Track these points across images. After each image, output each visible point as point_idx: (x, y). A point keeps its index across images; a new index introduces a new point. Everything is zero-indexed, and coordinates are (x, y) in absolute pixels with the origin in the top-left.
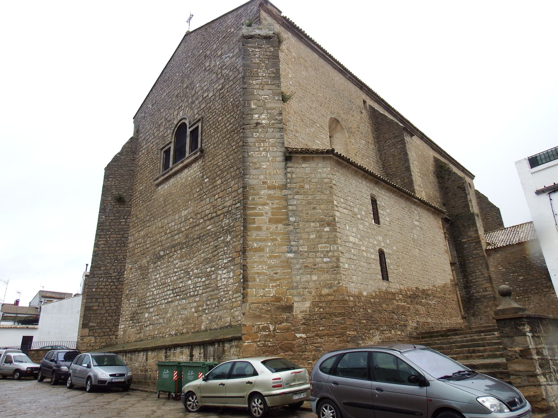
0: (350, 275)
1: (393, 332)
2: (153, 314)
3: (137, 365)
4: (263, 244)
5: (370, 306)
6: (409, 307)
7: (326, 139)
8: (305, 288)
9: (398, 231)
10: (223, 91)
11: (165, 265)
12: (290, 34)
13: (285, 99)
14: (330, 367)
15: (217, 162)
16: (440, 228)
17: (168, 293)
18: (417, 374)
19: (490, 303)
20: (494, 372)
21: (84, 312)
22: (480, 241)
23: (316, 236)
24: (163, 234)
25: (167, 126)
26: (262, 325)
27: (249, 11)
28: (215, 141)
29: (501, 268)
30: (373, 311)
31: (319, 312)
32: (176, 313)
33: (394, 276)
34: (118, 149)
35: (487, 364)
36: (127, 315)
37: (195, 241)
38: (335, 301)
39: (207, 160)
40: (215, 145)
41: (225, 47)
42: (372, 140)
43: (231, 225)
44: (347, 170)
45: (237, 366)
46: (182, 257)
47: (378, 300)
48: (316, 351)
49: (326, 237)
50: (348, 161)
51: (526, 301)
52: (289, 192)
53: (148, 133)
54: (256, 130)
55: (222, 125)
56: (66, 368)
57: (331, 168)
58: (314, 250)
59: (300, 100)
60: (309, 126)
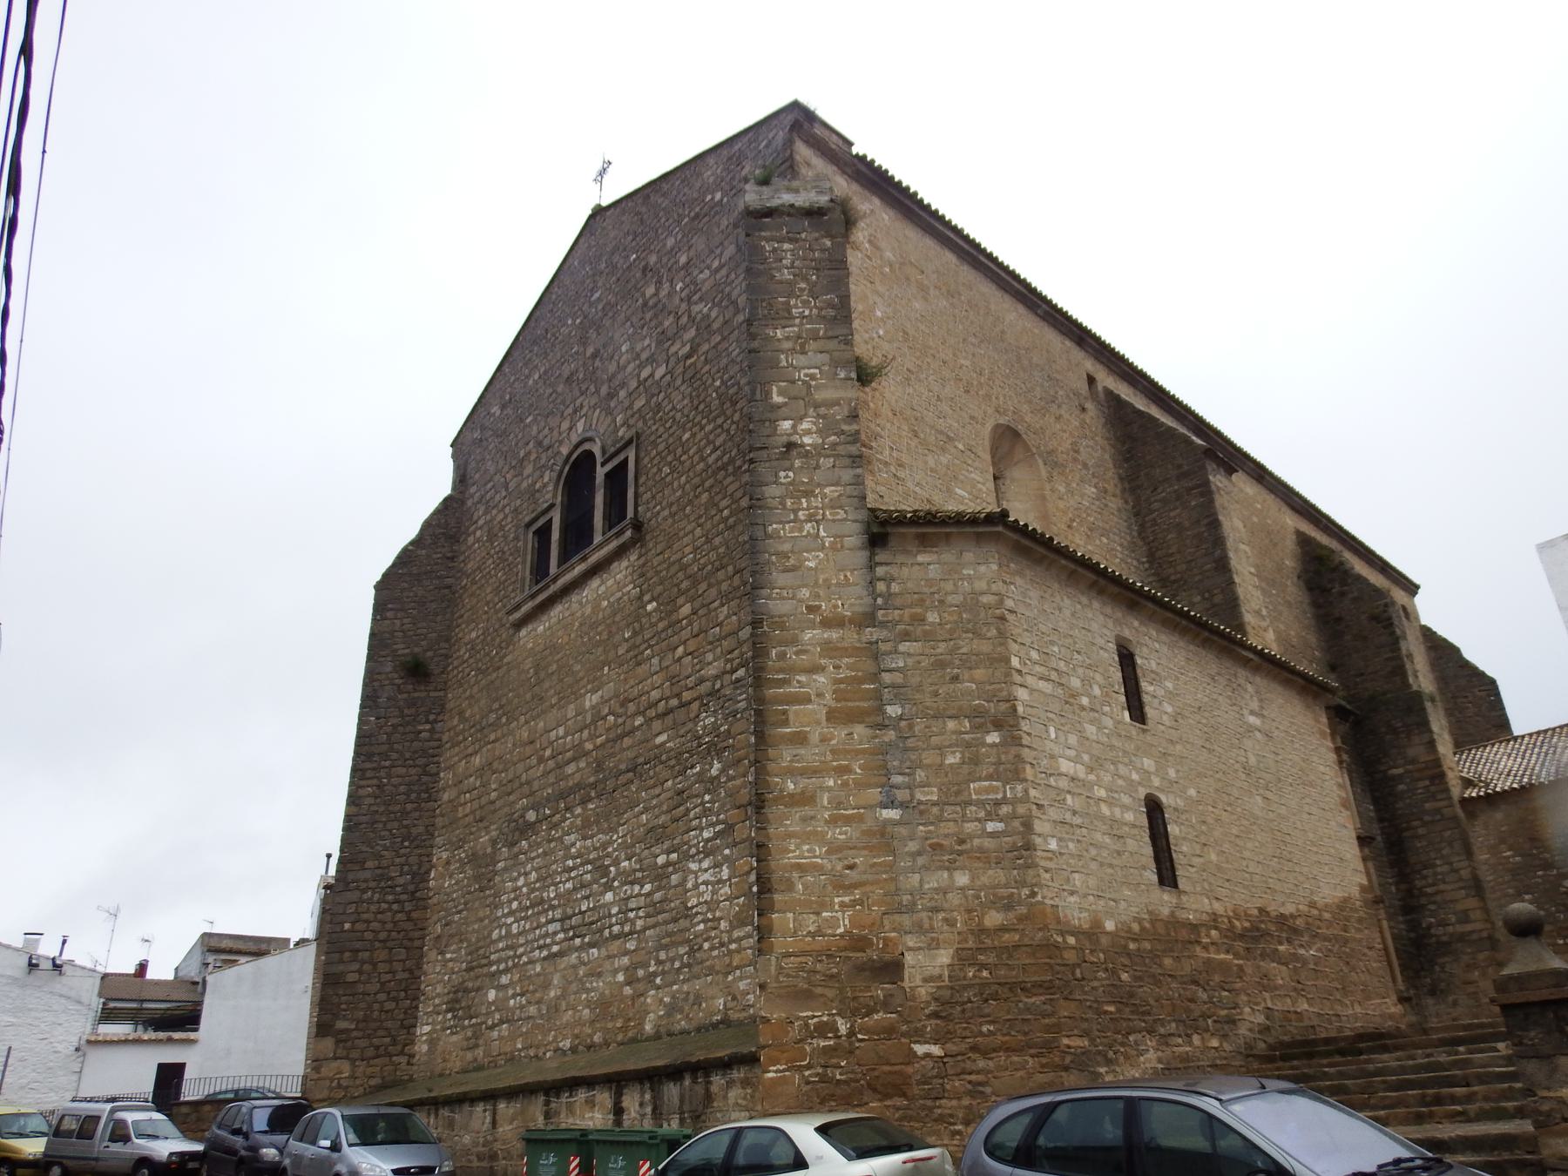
0: (1063, 872)
1: (1196, 1039)
2: (510, 992)
3: (467, 1139)
4: (813, 784)
5: (1127, 962)
6: (1240, 967)
7: (984, 484)
8: (936, 910)
9: (1201, 743)
10: (692, 360)
11: (540, 851)
12: (877, 201)
13: (865, 376)
14: (1014, 1144)
15: (679, 555)
16: (1322, 733)
17: (551, 928)
18: (1272, 1168)
19: (1481, 956)
20: (1498, 1162)
21: (323, 989)
22: (1442, 775)
23: (963, 757)
24: (534, 761)
25: (543, 462)
26: (816, 1020)
27: (764, 143)
28: (672, 499)
29: (1508, 853)
30: (1136, 978)
31: (977, 981)
32: (574, 987)
33: (1194, 875)
34: (411, 531)
35: (1476, 1136)
36: (438, 995)
37: (623, 779)
38: (1024, 949)
39: (653, 552)
40: (674, 508)
41: (699, 243)
42: (1116, 486)
43: (722, 729)
44: (1047, 570)
45: (748, 1140)
46: (586, 824)
47: (1147, 945)
48: (972, 1094)
49: (992, 760)
50: (1047, 543)
52: (884, 634)
53: (489, 486)
54: (787, 464)
55: (691, 452)
56: (273, 1151)
57: (1000, 566)
58: (959, 799)
59: (907, 379)
60: (934, 449)
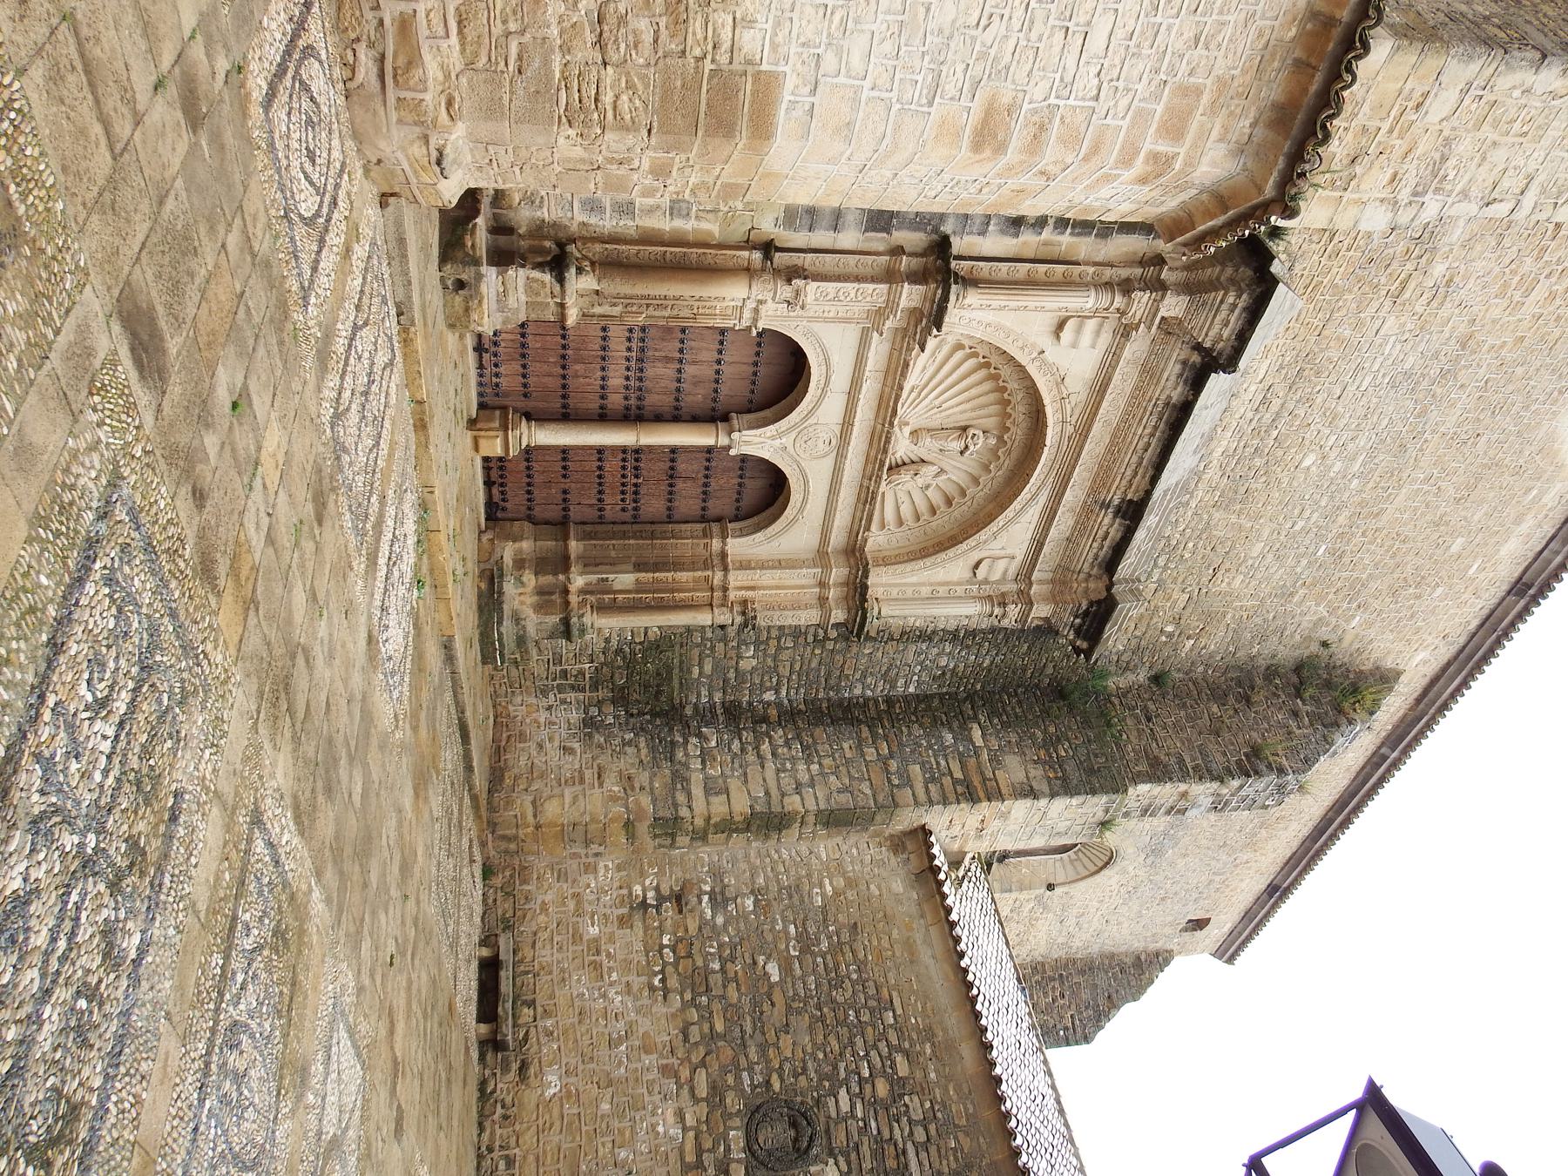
19: (645, 801)
29: (829, 888)
51: (644, 979)
